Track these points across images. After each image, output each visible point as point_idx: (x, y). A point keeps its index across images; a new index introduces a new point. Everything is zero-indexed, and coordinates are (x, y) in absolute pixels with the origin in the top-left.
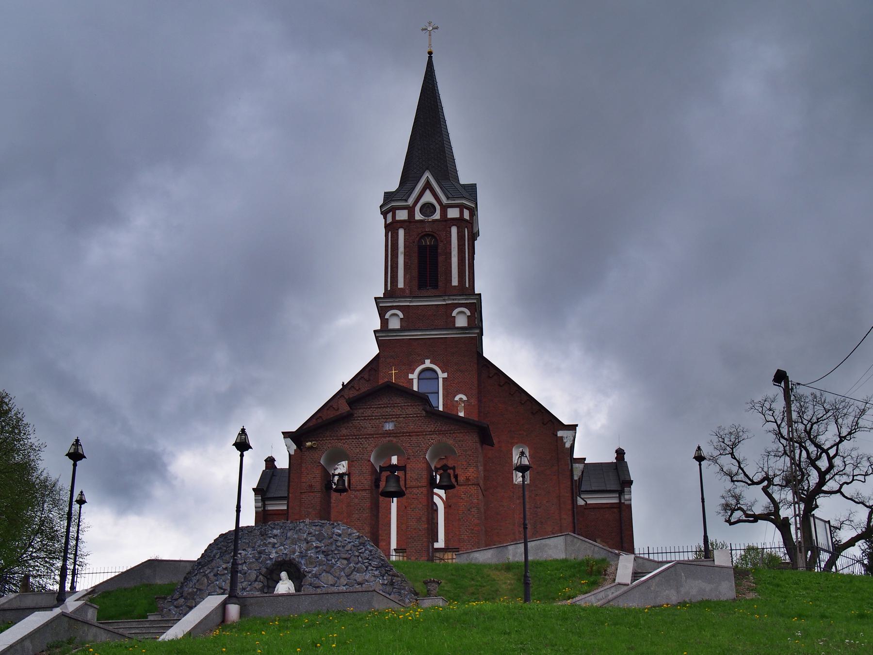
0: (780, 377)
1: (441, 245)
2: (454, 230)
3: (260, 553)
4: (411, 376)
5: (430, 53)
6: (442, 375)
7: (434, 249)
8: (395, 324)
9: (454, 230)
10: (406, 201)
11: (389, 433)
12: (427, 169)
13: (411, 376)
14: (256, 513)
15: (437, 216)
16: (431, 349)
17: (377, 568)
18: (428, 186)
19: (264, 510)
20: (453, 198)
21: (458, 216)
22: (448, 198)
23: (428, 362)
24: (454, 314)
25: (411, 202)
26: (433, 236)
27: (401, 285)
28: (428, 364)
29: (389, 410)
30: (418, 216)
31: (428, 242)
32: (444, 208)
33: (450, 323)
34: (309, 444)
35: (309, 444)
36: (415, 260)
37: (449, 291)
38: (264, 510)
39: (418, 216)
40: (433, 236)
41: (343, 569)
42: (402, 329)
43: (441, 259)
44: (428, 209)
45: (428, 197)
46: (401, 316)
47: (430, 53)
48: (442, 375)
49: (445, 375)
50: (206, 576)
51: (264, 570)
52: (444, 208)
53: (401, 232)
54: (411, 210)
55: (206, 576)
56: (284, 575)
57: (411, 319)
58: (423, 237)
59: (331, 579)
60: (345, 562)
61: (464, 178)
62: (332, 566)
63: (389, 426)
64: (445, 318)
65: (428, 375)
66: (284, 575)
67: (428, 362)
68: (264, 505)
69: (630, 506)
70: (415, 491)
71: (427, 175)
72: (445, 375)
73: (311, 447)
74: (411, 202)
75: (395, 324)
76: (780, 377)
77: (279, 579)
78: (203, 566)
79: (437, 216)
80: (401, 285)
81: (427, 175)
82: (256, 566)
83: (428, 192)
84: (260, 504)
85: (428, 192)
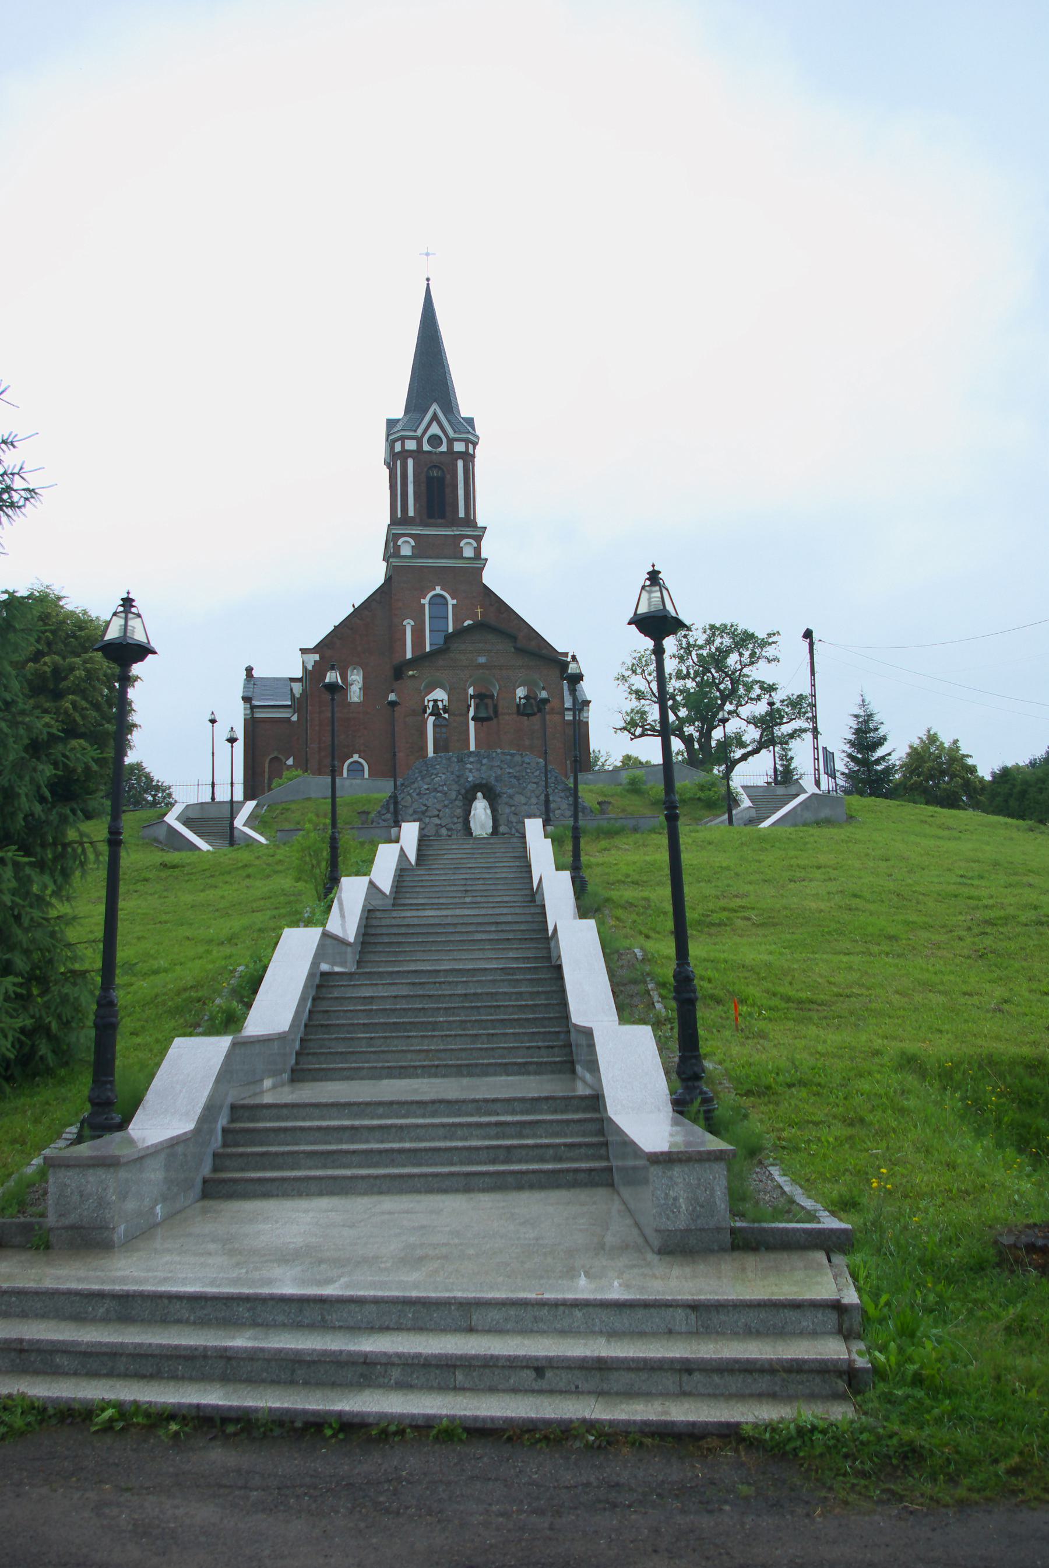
0: (808, 634)
1: (448, 477)
2: (460, 464)
3: (458, 777)
4: (423, 601)
5: (428, 280)
6: (451, 602)
7: (441, 481)
8: (406, 551)
9: (460, 464)
10: (415, 431)
11: (481, 666)
12: (435, 401)
13: (423, 601)
14: (245, 720)
15: (444, 448)
16: (441, 576)
17: (563, 791)
18: (435, 418)
19: (253, 718)
20: (460, 432)
21: (463, 450)
22: (455, 432)
23: (438, 588)
24: (462, 544)
25: (419, 432)
26: (440, 468)
27: (411, 513)
28: (438, 590)
29: (481, 645)
30: (426, 447)
31: (435, 473)
32: (451, 442)
33: (458, 554)
34: (411, 673)
35: (411, 673)
36: (423, 487)
37: (455, 522)
38: (253, 718)
39: (426, 447)
40: (440, 468)
41: (533, 791)
42: (412, 557)
43: (448, 490)
44: (435, 440)
45: (435, 429)
46: (413, 543)
47: (428, 280)
48: (451, 602)
49: (455, 602)
50: (410, 795)
51: (463, 791)
52: (451, 442)
53: (410, 462)
54: (419, 440)
55: (410, 795)
56: (479, 795)
57: (423, 547)
58: (430, 468)
59: (523, 800)
60: (535, 786)
61: (465, 413)
62: (524, 788)
63: (482, 660)
64: (452, 548)
65: (439, 600)
66: (479, 795)
67: (438, 588)
68: (252, 713)
69: (587, 723)
70: (507, 717)
71: (435, 407)
72: (455, 602)
73: (413, 676)
74: (419, 432)
75: (406, 551)
76: (808, 634)
77: (474, 798)
78: (406, 787)
79: (444, 448)
80: (411, 513)
81: (435, 407)
82: (455, 787)
83: (435, 423)
84: (248, 712)
85: (435, 423)
